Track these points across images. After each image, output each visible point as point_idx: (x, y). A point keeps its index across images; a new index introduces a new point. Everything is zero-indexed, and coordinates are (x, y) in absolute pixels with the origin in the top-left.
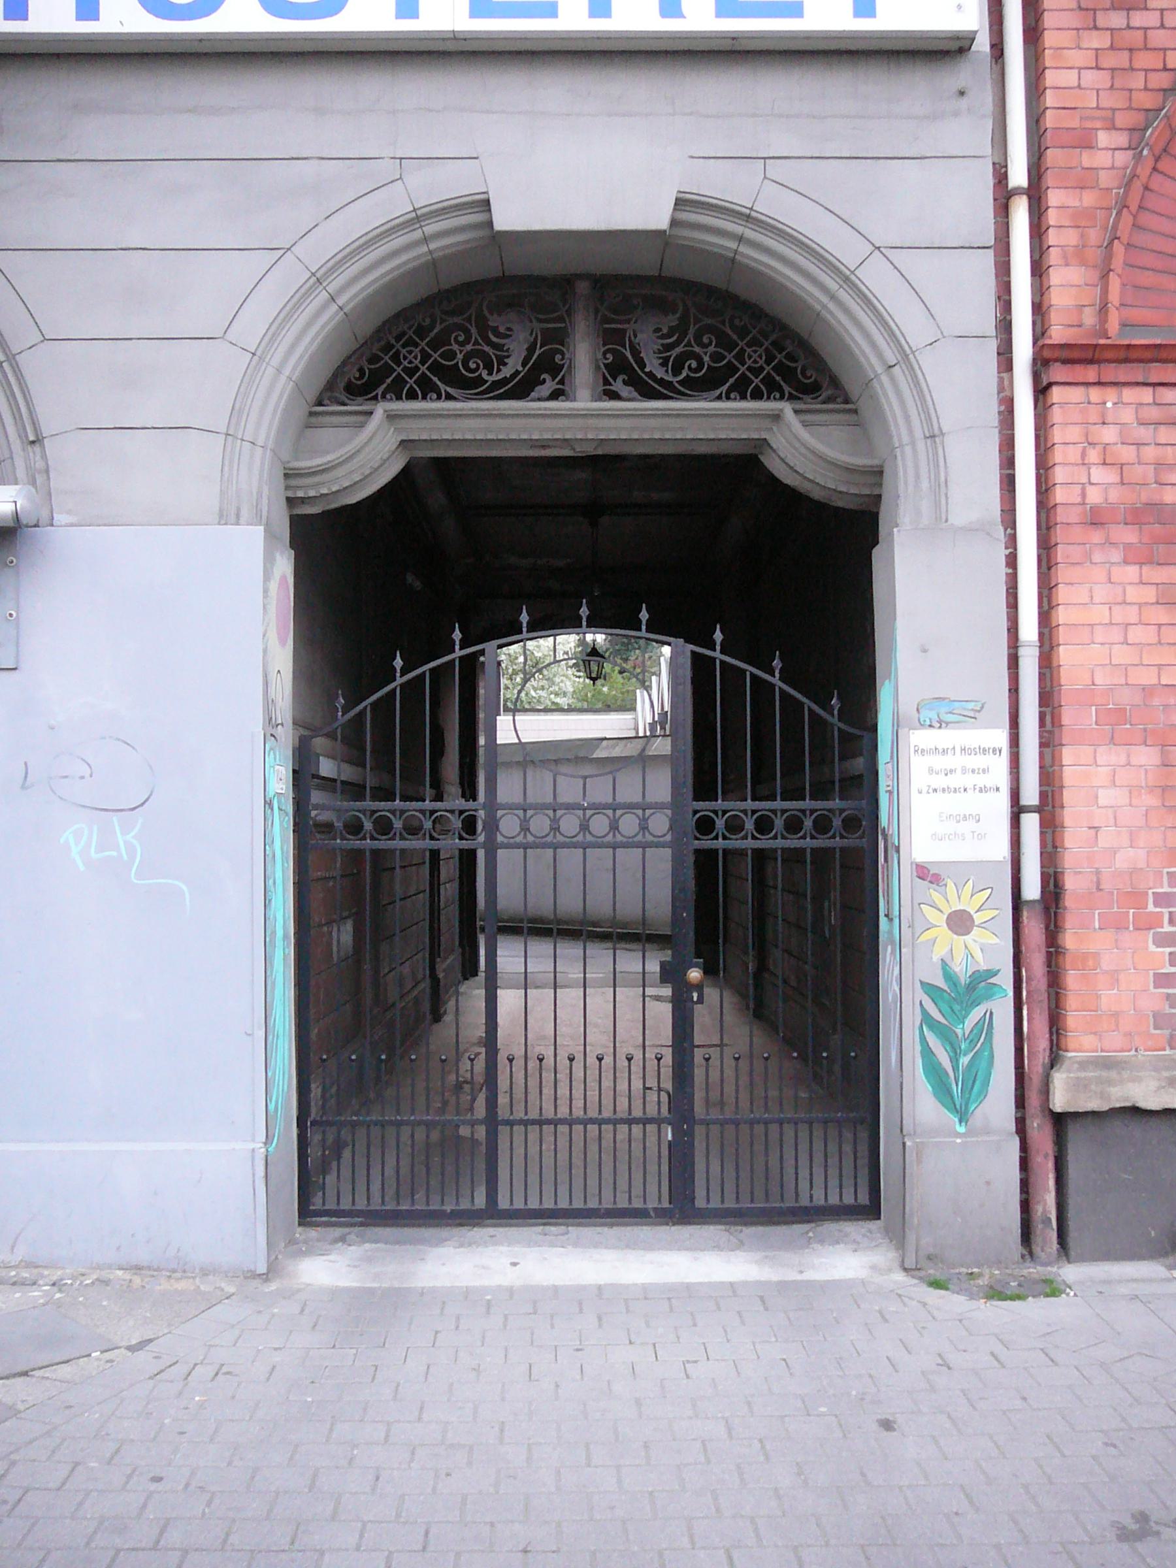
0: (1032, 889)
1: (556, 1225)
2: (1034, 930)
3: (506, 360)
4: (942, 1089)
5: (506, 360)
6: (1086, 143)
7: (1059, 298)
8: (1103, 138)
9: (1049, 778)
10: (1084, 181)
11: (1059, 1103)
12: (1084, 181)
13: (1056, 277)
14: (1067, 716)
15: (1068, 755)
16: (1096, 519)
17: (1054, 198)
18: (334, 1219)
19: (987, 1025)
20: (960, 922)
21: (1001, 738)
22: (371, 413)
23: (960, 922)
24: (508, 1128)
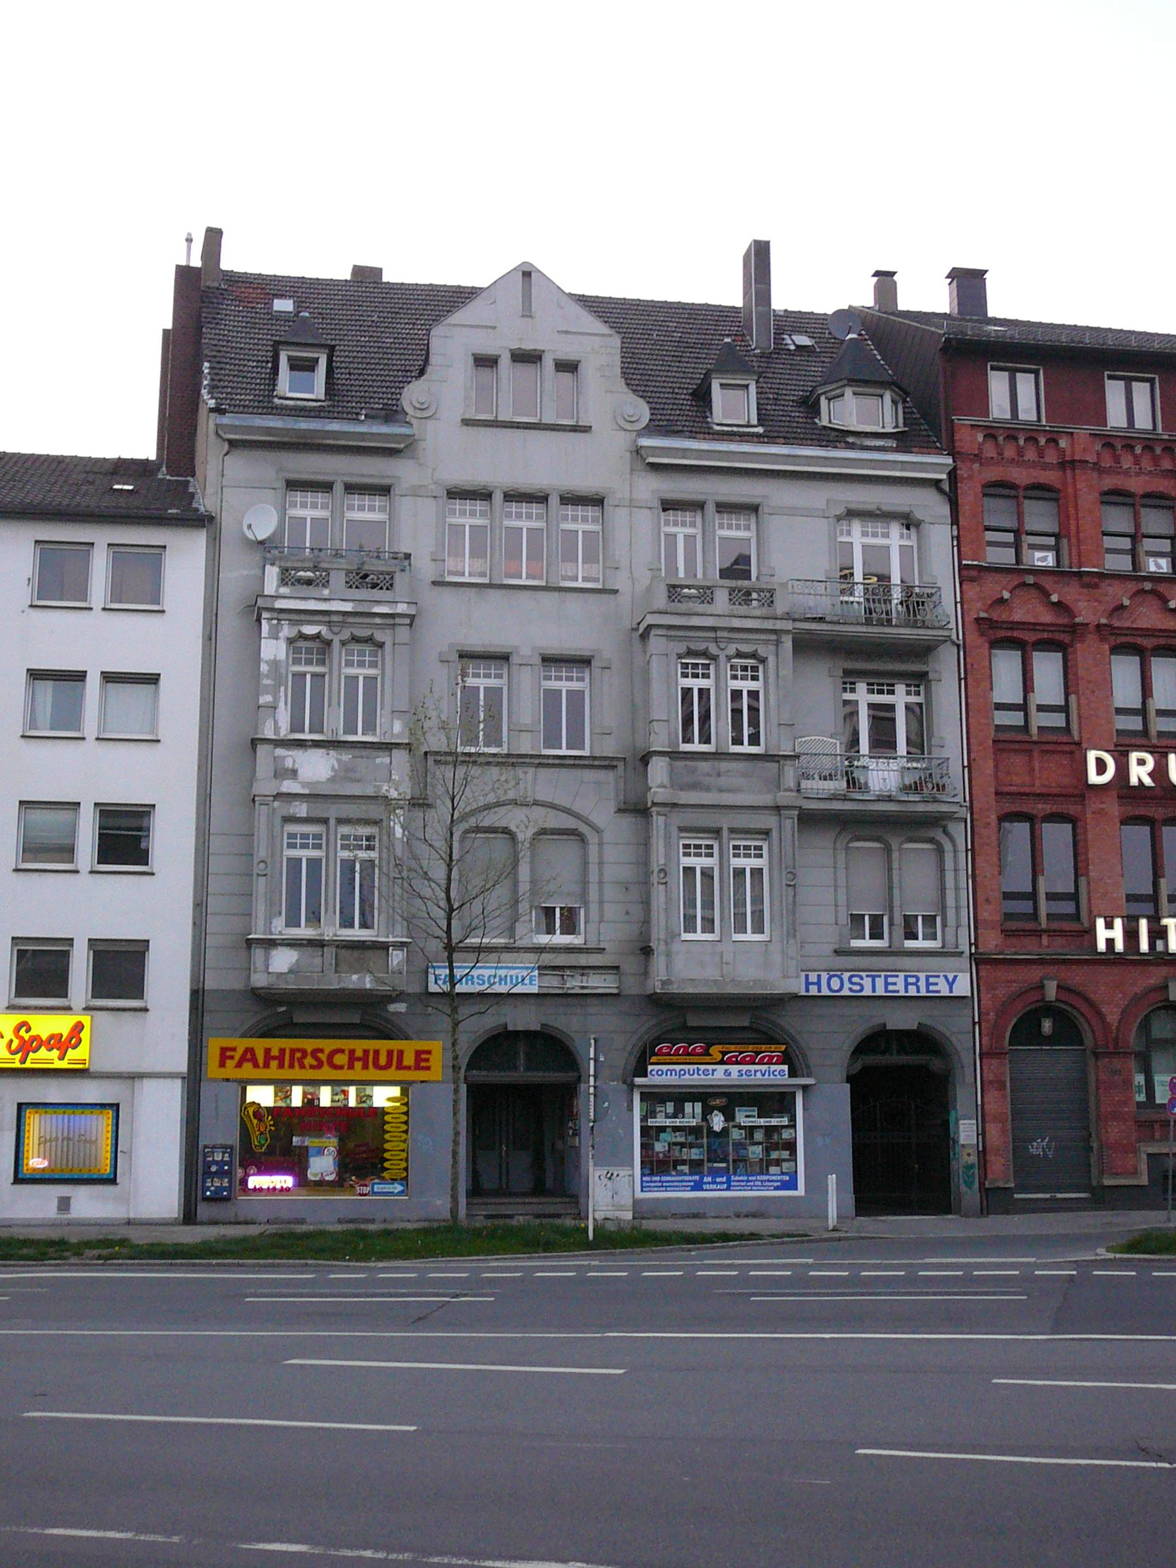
0: (981, 1149)
1: (182, 1092)
2: (981, 1155)
3: (950, 280)
4: (966, 1186)
5: (950, 280)
6: (988, 1014)
7: (983, 1042)
8: (991, 1014)
9: (983, 1128)
10: (988, 1021)
11: (987, 1186)
12: (988, 1021)
13: (983, 1040)
14: (987, 1118)
15: (987, 1125)
16: (990, 1082)
17: (983, 1024)
18: (291, 1261)
19: (973, 1173)
20: (969, 1155)
21: (975, 1122)
22: (843, 395)
23: (969, 1155)
24: (1026, 826)
